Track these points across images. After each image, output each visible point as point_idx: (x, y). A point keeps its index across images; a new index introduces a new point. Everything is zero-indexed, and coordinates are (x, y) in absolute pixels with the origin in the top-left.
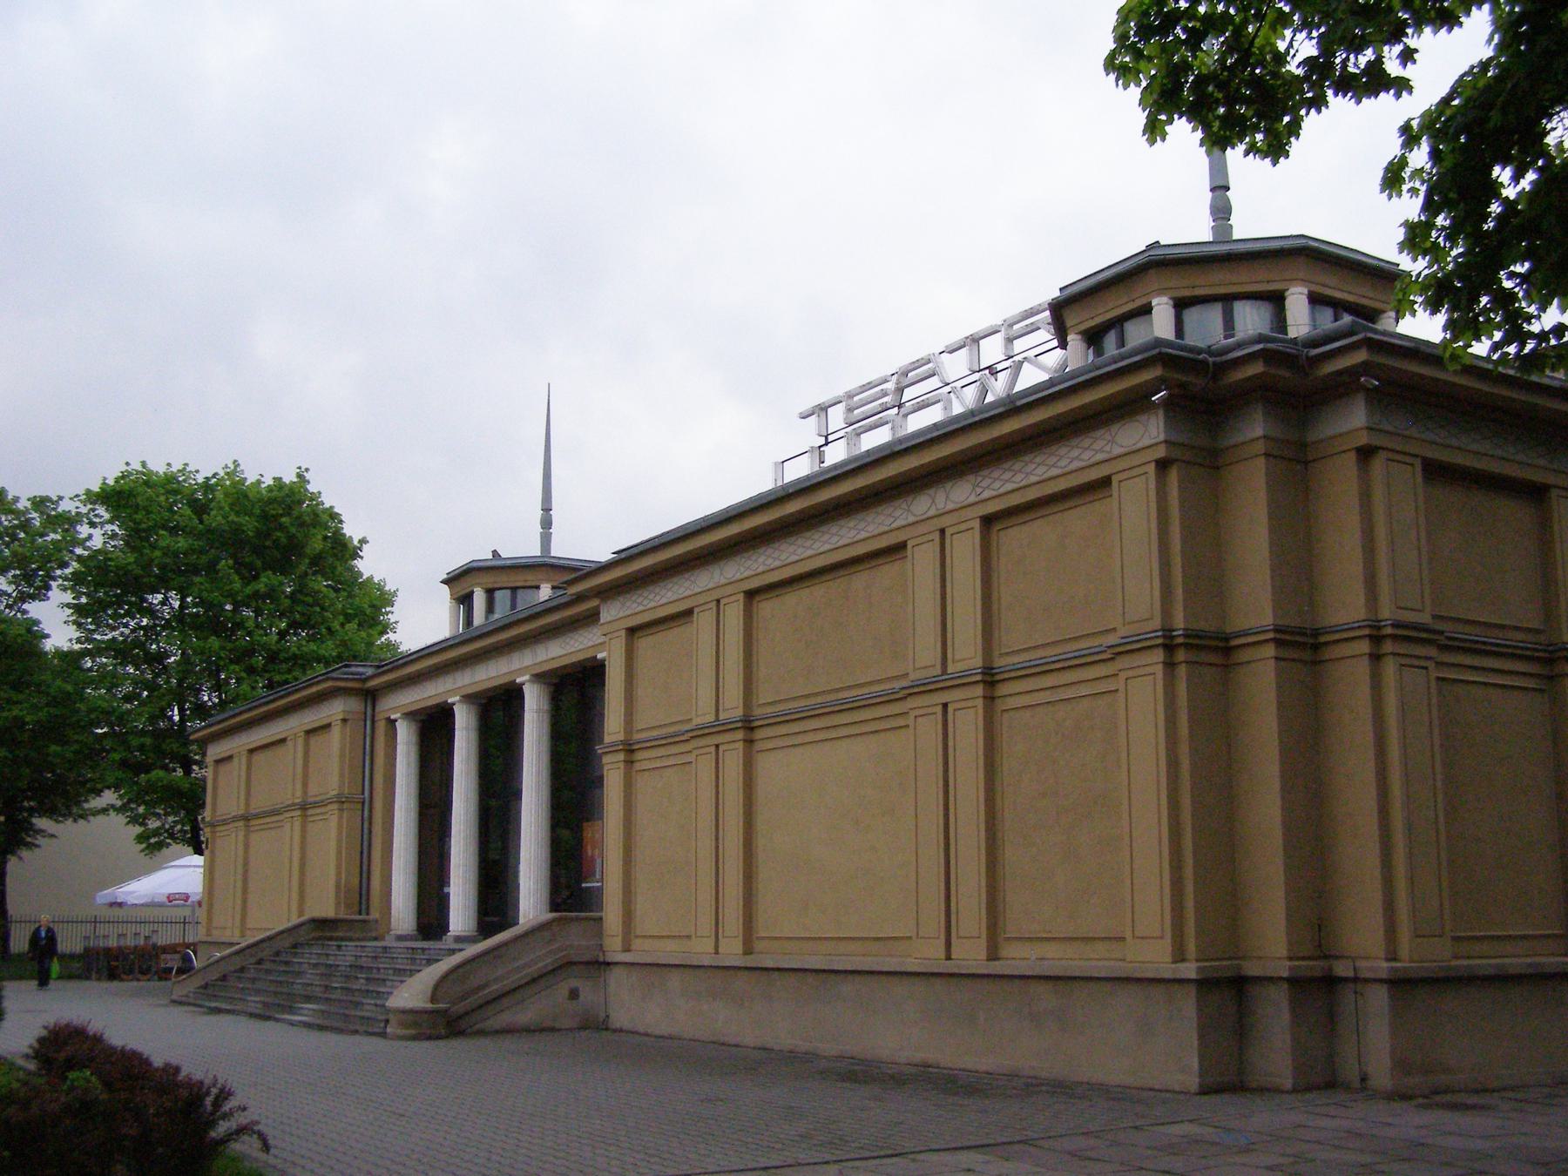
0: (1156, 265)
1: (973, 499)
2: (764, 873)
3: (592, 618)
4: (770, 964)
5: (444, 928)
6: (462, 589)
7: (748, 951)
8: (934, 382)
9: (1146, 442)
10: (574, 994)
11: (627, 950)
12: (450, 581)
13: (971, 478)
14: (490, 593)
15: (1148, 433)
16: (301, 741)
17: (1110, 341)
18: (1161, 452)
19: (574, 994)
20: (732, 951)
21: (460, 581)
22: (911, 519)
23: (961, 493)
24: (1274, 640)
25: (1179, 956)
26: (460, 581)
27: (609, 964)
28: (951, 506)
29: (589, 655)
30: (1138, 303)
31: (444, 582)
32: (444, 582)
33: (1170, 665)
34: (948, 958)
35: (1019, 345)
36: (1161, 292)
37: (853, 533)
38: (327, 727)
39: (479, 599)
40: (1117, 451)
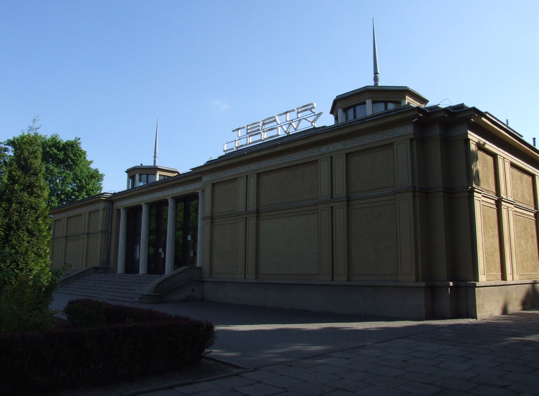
0: (365, 92)
1: (343, 148)
2: (498, 265)
3: (200, 179)
4: (275, 282)
5: (116, 271)
6: (132, 174)
7: (257, 278)
8: (275, 123)
9: (406, 133)
10: (193, 290)
11: (210, 277)
12: (128, 171)
13: (343, 142)
14: (140, 175)
15: (408, 130)
16: (87, 215)
17: (351, 112)
18: (412, 136)
19: (193, 290)
20: (251, 277)
21: (132, 173)
22: (320, 153)
23: (339, 146)
24: (443, 191)
25: (417, 280)
26: (132, 173)
27: (204, 281)
28: (334, 150)
29: (194, 191)
30: (362, 101)
31: (126, 172)
32: (126, 172)
33: (414, 197)
34: (333, 280)
35: (299, 115)
36: (369, 98)
37: (298, 157)
38: (98, 211)
39: (137, 177)
40: (396, 135)
